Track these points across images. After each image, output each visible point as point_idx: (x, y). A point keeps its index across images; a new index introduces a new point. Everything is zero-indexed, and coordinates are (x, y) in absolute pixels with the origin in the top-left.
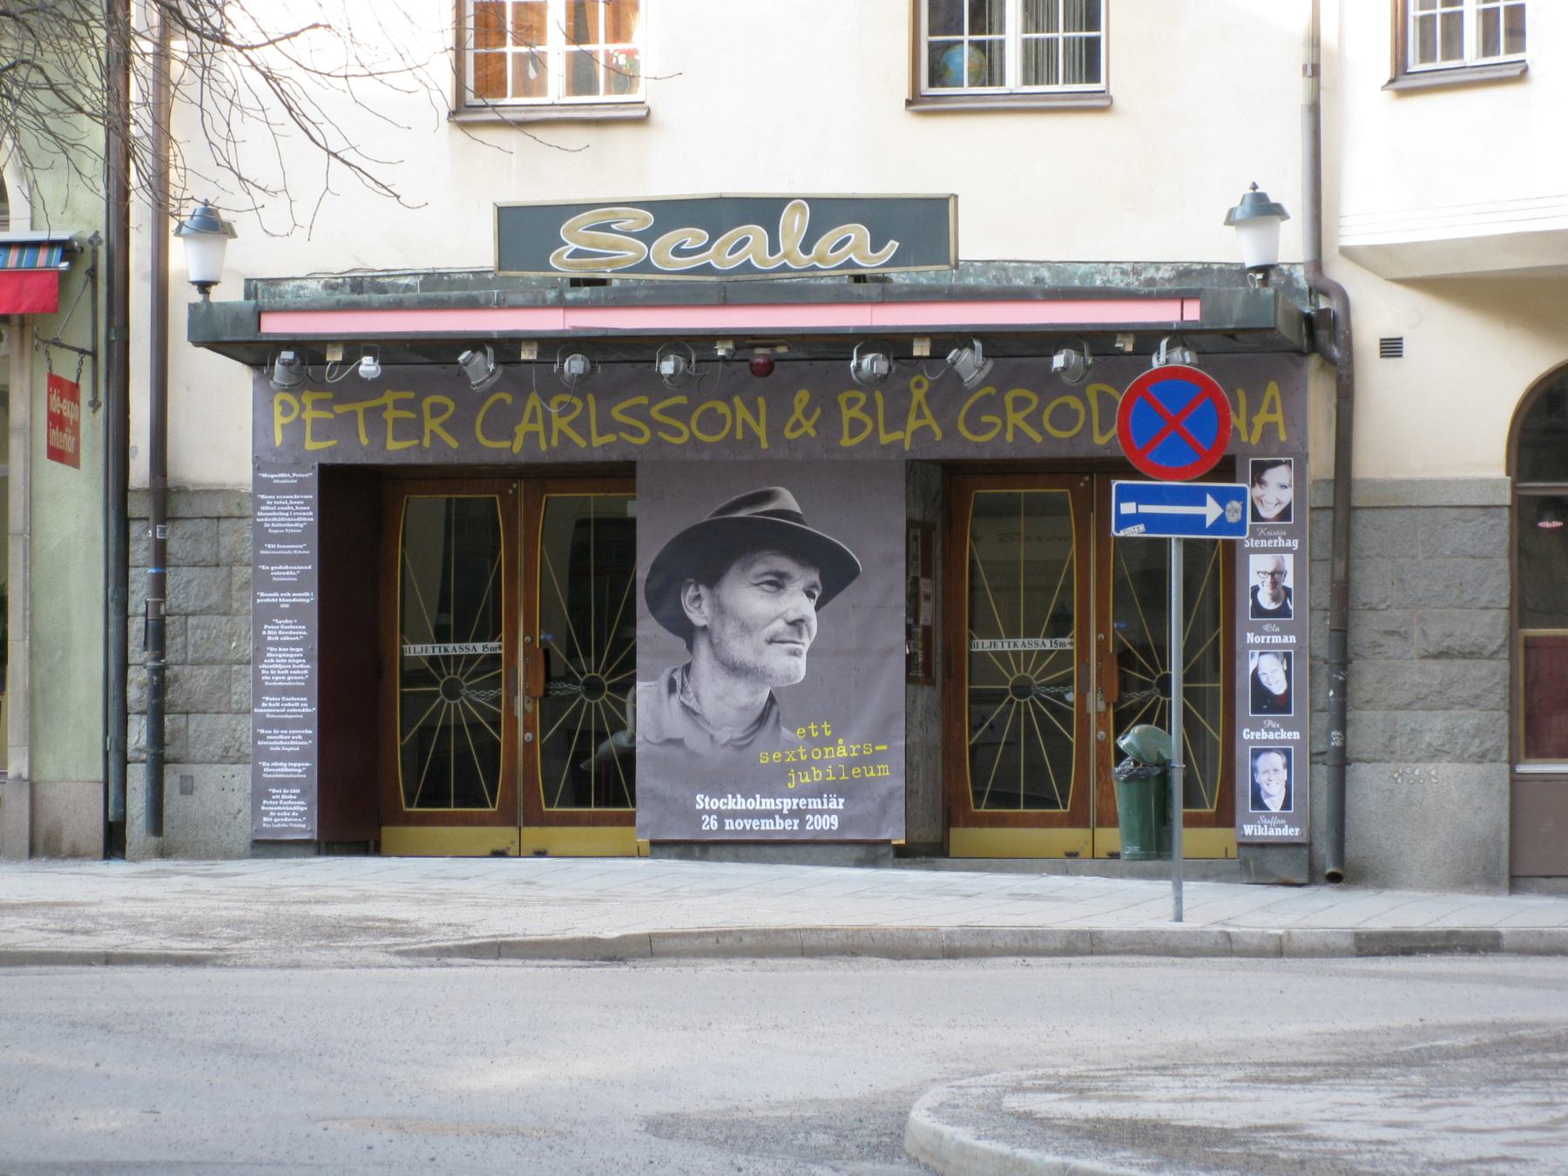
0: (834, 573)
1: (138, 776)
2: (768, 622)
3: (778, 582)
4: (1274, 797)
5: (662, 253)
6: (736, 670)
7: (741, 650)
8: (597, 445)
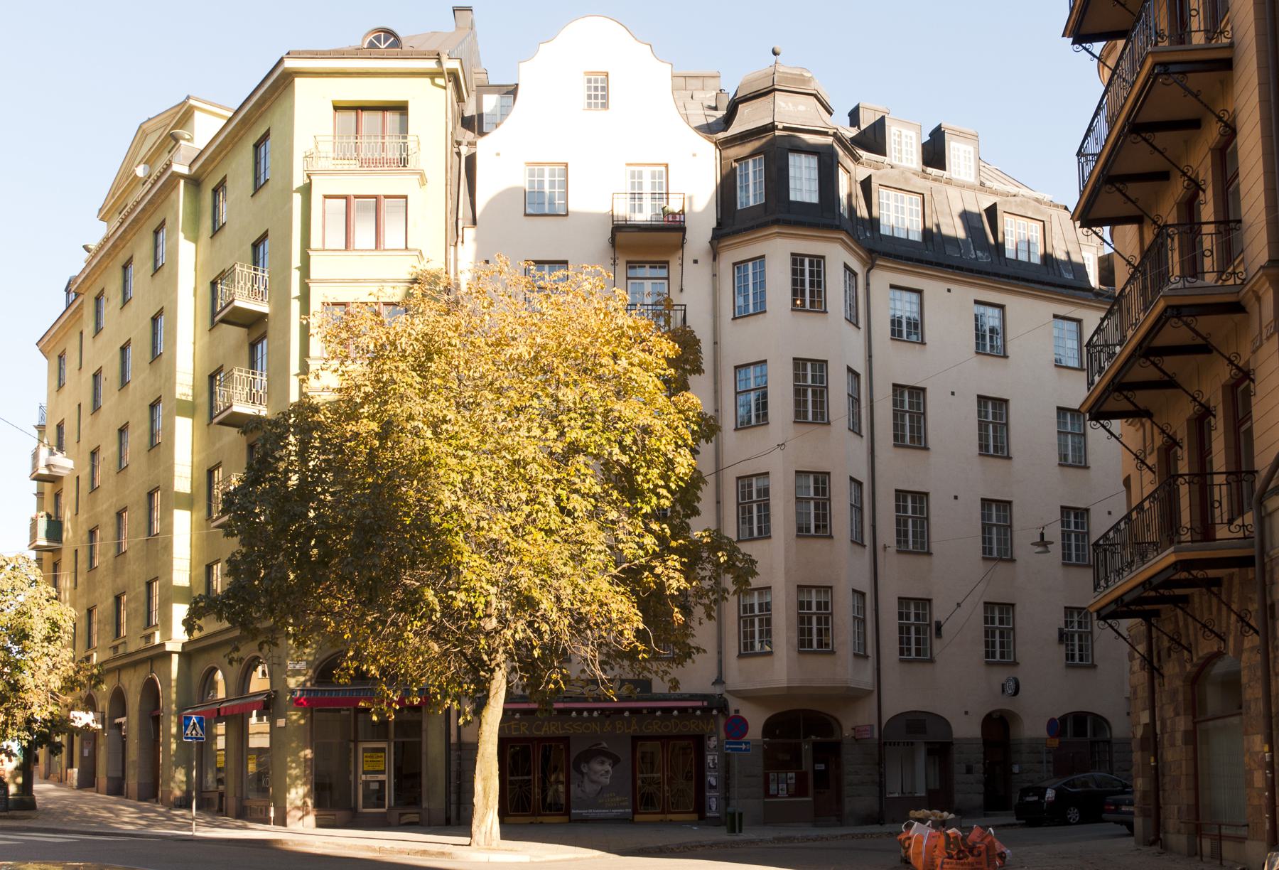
0: (615, 761)
1: (453, 807)
2: (601, 771)
3: (603, 763)
4: (714, 807)
5: (586, 691)
6: (593, 782)
7: (595, 778)
8: (561, 733)
